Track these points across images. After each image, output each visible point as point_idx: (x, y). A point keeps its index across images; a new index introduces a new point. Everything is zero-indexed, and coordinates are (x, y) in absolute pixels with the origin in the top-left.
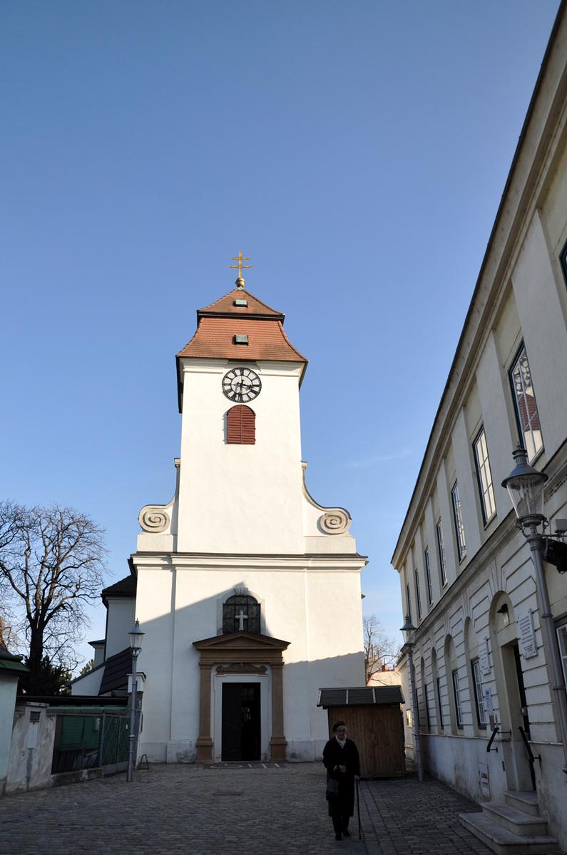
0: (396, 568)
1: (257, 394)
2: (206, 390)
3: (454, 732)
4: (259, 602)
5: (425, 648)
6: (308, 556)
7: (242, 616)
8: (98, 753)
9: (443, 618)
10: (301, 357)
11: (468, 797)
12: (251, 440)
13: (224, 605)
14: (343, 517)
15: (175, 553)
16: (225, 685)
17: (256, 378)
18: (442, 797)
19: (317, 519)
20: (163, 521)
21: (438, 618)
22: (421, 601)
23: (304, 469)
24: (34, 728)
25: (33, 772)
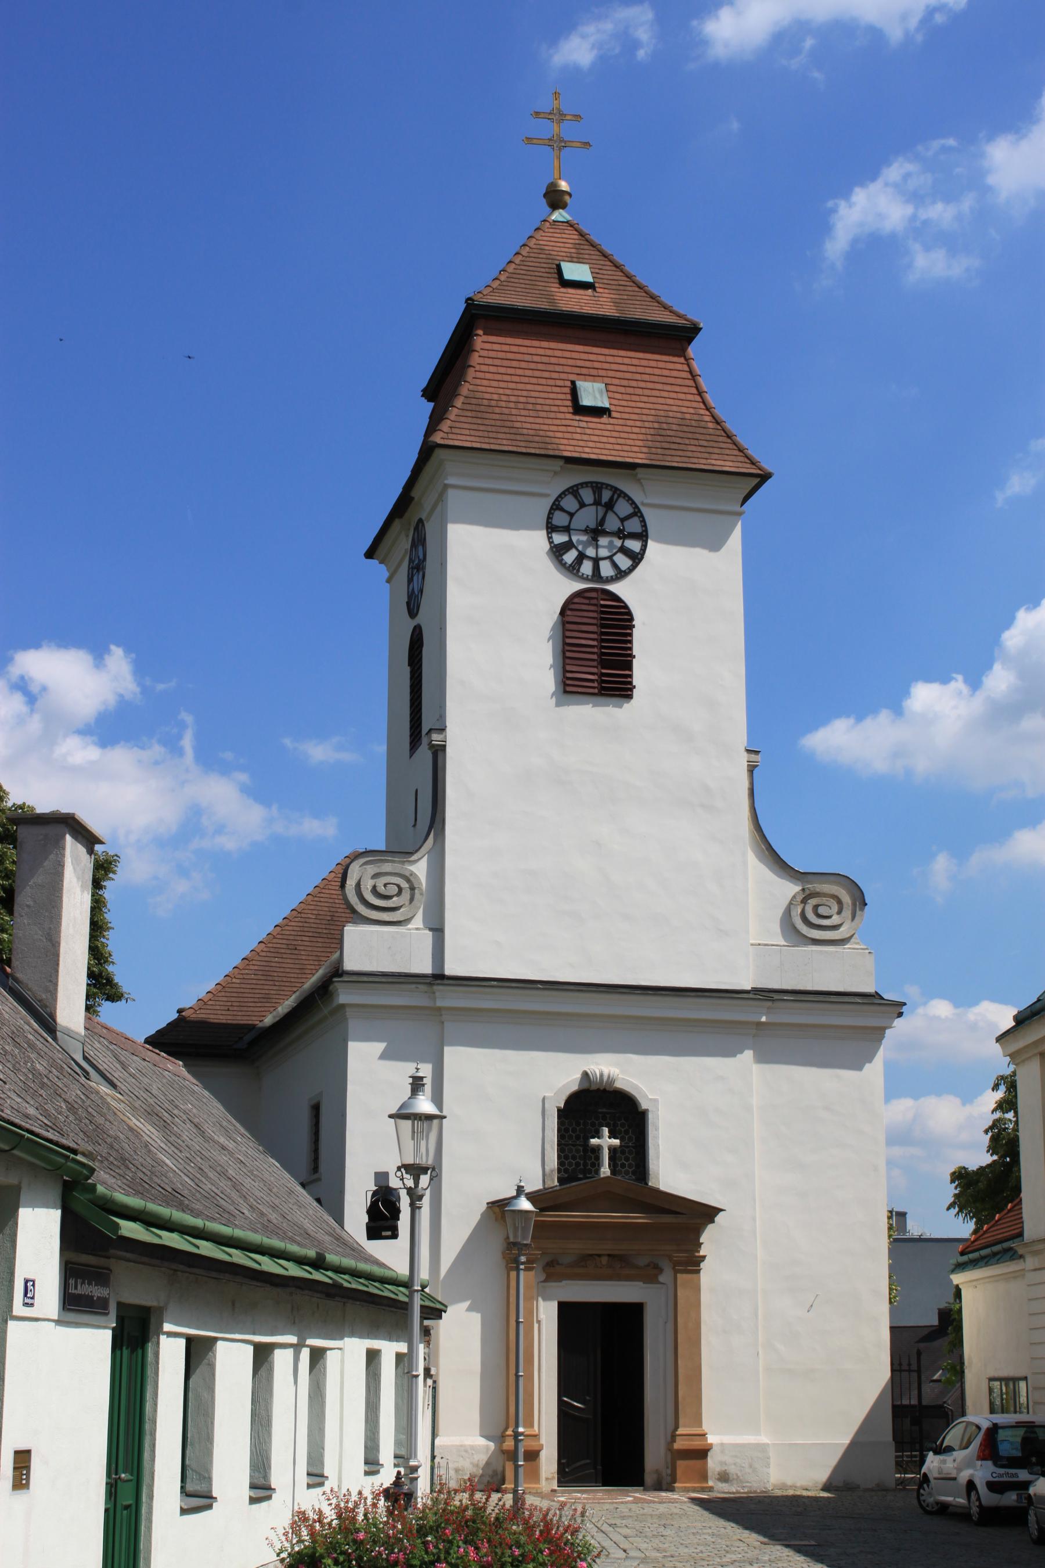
2: (501, 582)
4: (644, 1105)
6: (763, 995)
7: (606, 1141)
10: (753, 463)
14: (846, 899)
15: (439, 977)
19: (780, 911)
20: (406, 895)
23: (751, 769)
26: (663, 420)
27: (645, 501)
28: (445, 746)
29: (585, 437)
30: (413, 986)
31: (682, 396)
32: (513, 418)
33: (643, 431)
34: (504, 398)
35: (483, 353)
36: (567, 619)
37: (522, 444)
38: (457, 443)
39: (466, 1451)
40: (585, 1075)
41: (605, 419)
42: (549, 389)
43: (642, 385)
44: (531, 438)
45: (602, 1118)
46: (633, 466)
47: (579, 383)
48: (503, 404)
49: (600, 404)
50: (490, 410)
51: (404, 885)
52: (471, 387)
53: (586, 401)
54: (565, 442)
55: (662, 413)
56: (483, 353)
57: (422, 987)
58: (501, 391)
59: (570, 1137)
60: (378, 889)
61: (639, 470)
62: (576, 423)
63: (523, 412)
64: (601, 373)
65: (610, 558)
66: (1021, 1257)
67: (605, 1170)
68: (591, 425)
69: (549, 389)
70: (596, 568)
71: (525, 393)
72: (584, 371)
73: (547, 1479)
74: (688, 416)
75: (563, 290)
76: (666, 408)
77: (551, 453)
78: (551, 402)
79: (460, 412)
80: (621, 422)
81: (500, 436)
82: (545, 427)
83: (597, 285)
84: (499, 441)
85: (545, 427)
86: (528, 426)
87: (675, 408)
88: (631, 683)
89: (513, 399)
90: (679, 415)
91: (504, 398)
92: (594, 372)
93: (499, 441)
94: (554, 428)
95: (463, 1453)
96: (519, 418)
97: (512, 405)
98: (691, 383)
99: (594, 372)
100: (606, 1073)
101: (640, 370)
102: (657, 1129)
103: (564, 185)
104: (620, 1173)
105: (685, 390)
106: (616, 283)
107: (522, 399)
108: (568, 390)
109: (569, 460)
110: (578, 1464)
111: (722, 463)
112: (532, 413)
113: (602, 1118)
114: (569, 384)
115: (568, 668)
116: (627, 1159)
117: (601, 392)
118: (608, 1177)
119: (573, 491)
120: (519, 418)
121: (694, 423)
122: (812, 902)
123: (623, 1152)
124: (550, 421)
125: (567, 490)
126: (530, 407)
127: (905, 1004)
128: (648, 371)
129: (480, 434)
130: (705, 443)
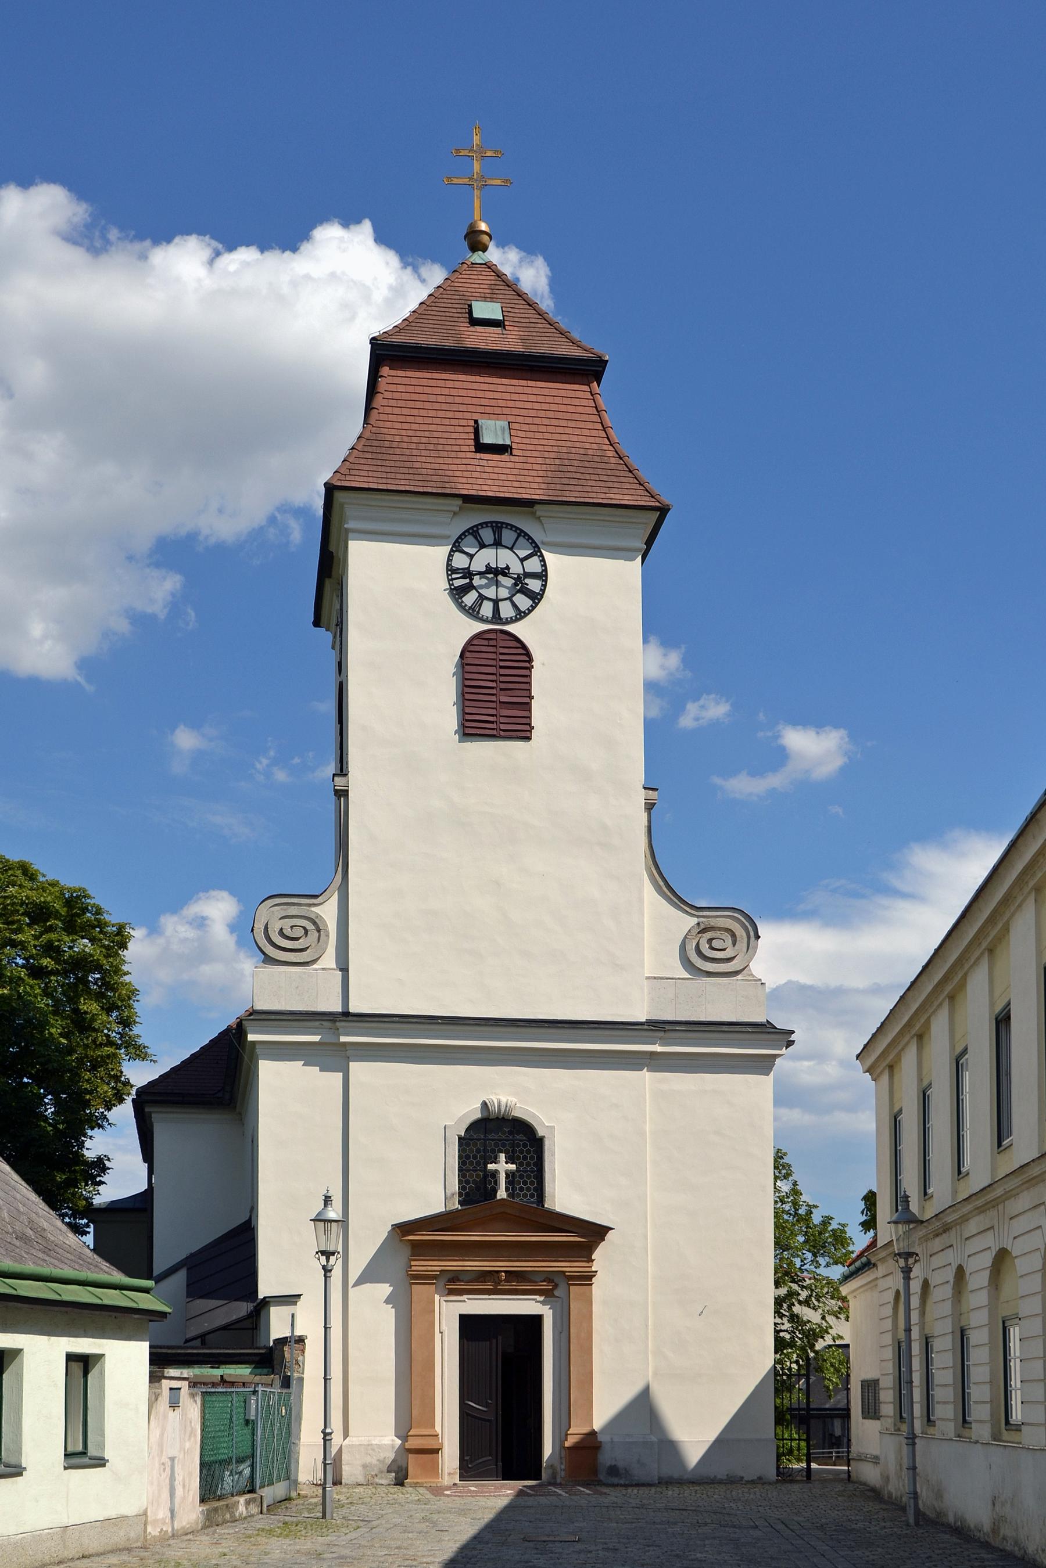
0: (869, 1070)
1: (536, 598)
3: (996, 1437)
4: (541, 1133)
5: (937, 1261)
6: (656, 1028)
7: (502, 1166)
8: (253, 1466)
9: (993, 1213)
11: (1018, 1553)
12: (523, 732)
13: (460, 1138)
14: (740, 932)
15: (346, 1014)
16: (466, 1321)
17: (519, 536)
18: (966, 1553)
20: (313, 935)
21: (981, 1210)
22: (933, 1156)
23: (650, 807)
24: (173, 1416)
25: (177, 1500)
26: (565, 456)
27: (546, 539)
28: (347, 791)
29: (485, 476)
30: (317, 1023)
31: (586, 432)
32: (414, 459)
33: (544, 467)
34: (406, 439)
35: (389, 395)
36: (466, 661)
37: (420, 484)
38: (354, 484)
39: (373, 1450)
40: (484, 1104)
41: (505, 457)
42: (452, 429)
43: (546, 422)
44: (429, 478)
45: (501, 1145)
46: (529, 504)
47: (480, 422)
48: (405, 445)
49: (501, 442)
50: (391, 451)
51: (310, 927)
52: (374, 430)
53: (487, 439)
54: (464, 480)
55: (564, 450)
56: (389, 395)
57: (325, 1024)
58: (404, 433)
59: (471, 1163)
60: (285, 931)
61: (537, 507)
62: (476, 462)
63: (424, 453)
64: (506, 411)
65: (510, 599)
66: (875, 1265)
67: (502, 1194)
68: (491, 463)
69: (452, 429)
70: (496, 610)
71: (427, 434)
72: (488, 410)
73: (449, 1474)
74: (590, 452)
75: (472, 329)
76: (569, 444)
77: (448, 491)
78: (453, 442)
79: (361, 455)
80: (522, 459)
81: (399, 476)
82: (445, 467)
83: (506, 323)
84: (397, 482)
85: (445, 467)
86: (428, 466)
87: (578, 445)
88: (530, 724)
89: (414, 440)
90: (582, 451)
91: (406, 439)
92: (498, 410)
93: (397, 482)
94: (455, 467)
95: (370, 1452)
96: (419, 459)
97: (414, 446)
98: (597, 419)
99: (498, 410)
100: (504, 1100)
101: (545, 406)
102: (553, 1155)
103: (483, 226)
104: (519, 1195)
105: (590, 425)
106: (527, 320)
107: (424, 440)
108: (472, 430)
109: (468, 499)
110: (480, 1461)
111: (621, 497)
112: (432, 453)
113: (501, 1145)
114: (472, 423)
115: (468, 710)
116: (525, 1183)
117: (503, 430)
118: (503, 1199)
119: (473, 531)
120: (419, 459)
121: (596, 459)
122: (709, 935)
123: (521, 1177)
124: (450, 461)
125: (467, 531)
126: (431, 447)
127: (793, 1032)
128: (554, 407)
129: (379, 475)
130: (605, 478)
